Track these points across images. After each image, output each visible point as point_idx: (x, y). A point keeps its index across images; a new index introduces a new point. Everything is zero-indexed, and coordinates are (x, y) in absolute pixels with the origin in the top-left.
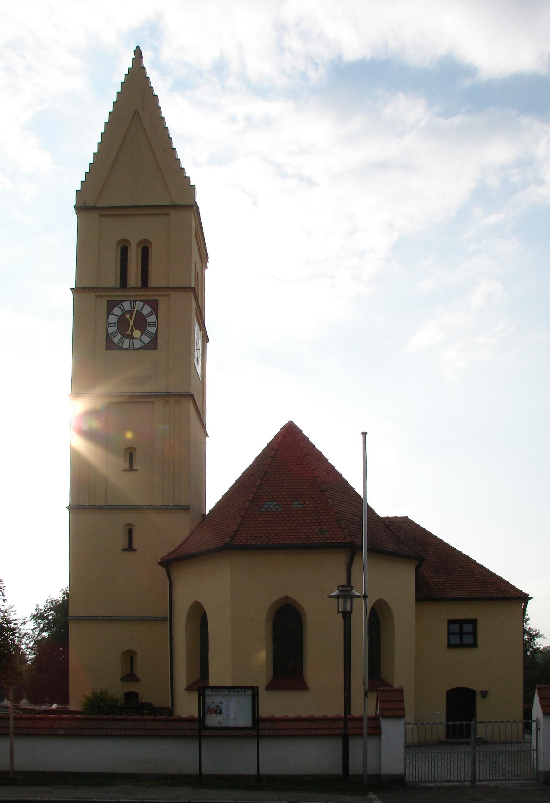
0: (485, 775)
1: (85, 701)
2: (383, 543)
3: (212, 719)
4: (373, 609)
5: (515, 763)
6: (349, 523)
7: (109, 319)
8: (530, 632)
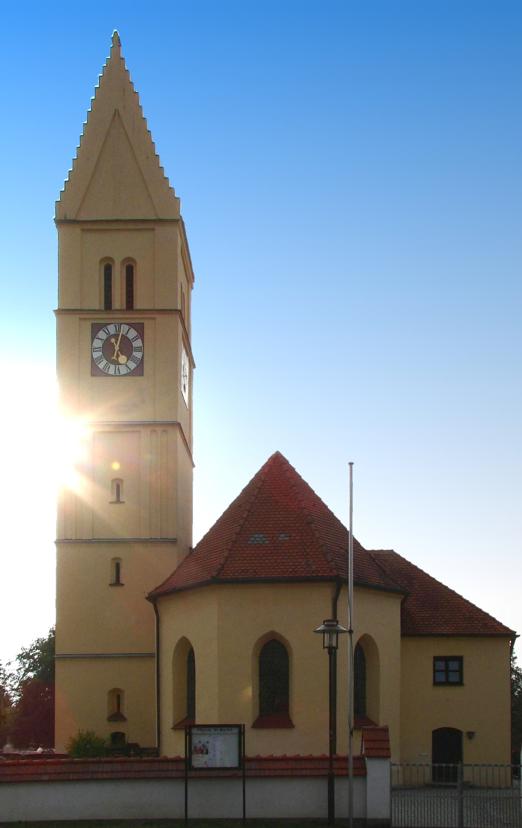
0: (472, 823)
1: (70, 743)
2: (369, 577)
4: (358, 644)
5: (503, 811)
6: (335, 556)
8: (518, 671)
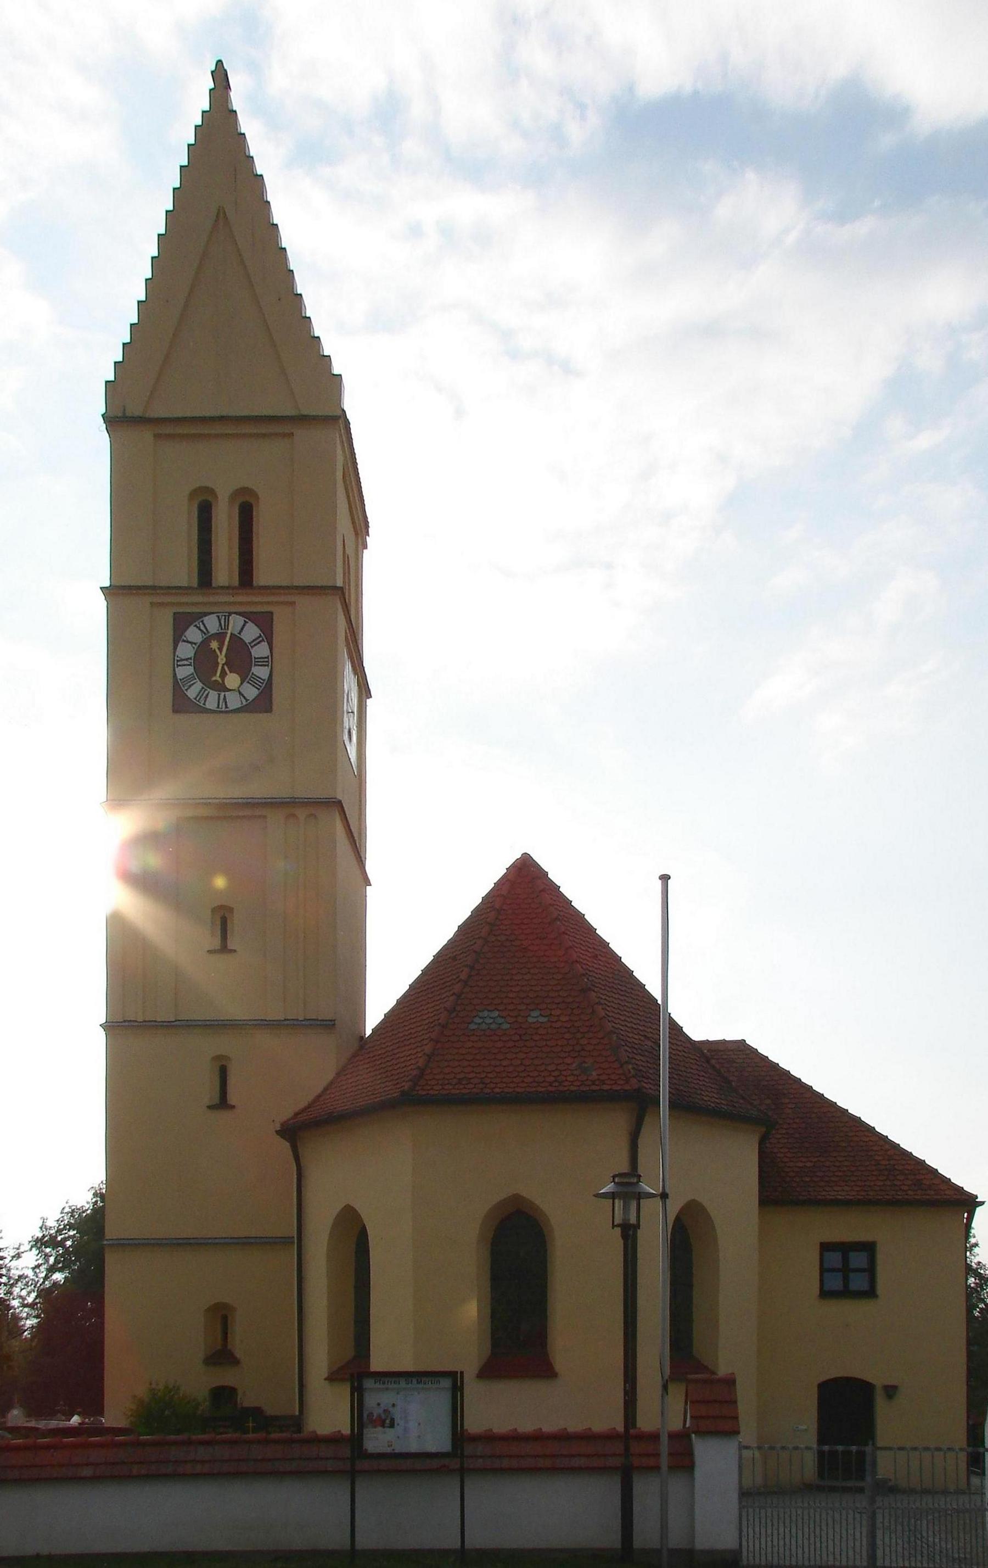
0: (894, 1557)
2: (699, 1092)
3: (375, 1437)
4: (678, 1219)
7: (178, 650)
8: (979, 1271)
